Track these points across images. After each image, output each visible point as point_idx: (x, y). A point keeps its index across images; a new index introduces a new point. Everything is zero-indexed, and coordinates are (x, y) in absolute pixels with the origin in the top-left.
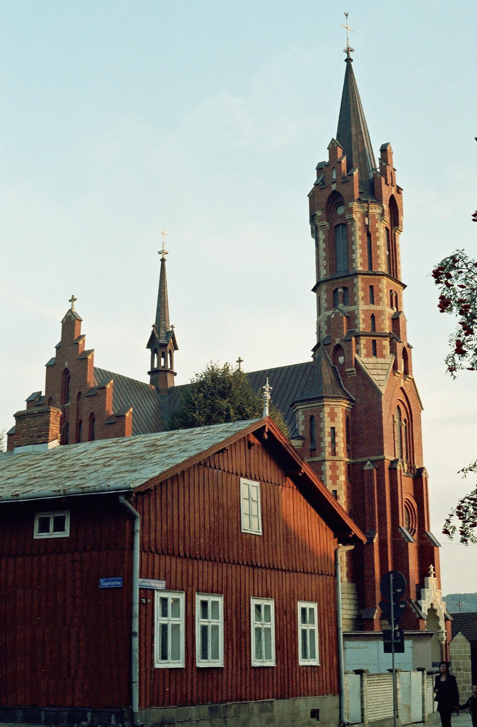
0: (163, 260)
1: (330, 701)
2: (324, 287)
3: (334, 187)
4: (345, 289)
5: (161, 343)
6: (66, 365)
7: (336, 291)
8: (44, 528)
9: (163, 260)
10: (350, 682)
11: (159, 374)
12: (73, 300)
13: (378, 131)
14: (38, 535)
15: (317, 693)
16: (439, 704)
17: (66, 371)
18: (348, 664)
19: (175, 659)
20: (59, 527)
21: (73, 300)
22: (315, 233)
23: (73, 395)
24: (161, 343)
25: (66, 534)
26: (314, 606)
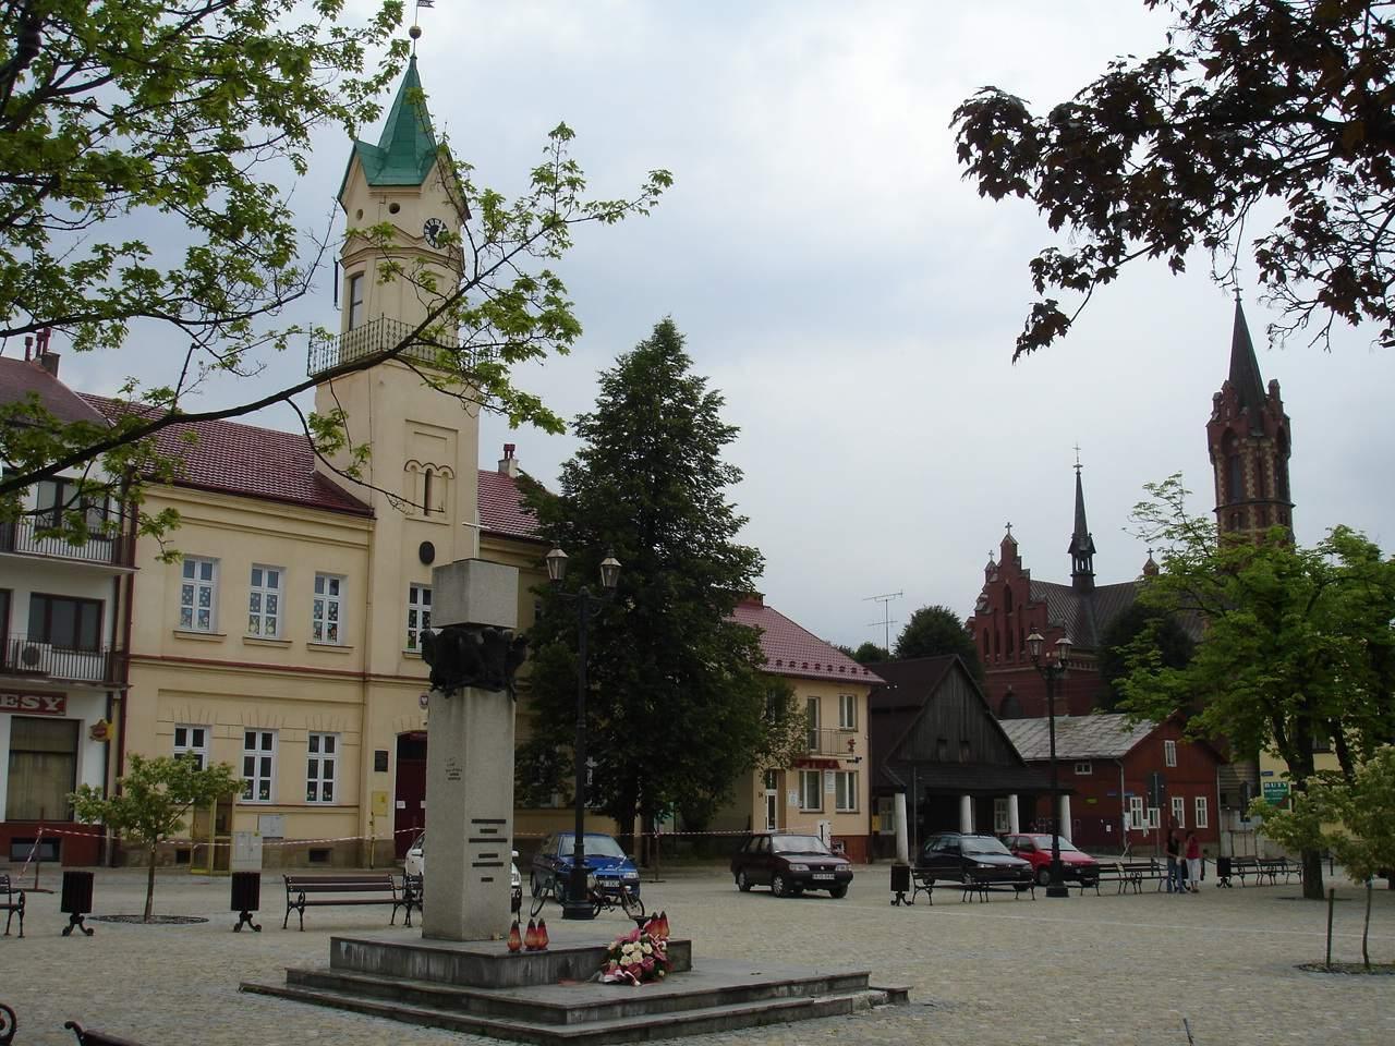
0: (1078, 473)
1: (1215, 846)
2: (1222, 512)
3: (1228, 424)
4: (1240, 513)
5: (1082, 547)
6: (1007, 581)
7: (1232, 516)
8: (1080, 770)
9: (1078, 473)
10: (1225, 836)
11: (1083, 576)
12: (1009, 526)
13: (1269, 366)
14: (1078, 773)
15: (371, 529)
16: (1019, 798)
17: (1007, 587)
18: (36, 884)
19: (181, 730)
20: (1087, 769)
21: (1009, 526)
22: (1213, 459)
23: (1015, 608)
24: (1082, 547)
25: (1091, 773)
26: (1205, 798)
